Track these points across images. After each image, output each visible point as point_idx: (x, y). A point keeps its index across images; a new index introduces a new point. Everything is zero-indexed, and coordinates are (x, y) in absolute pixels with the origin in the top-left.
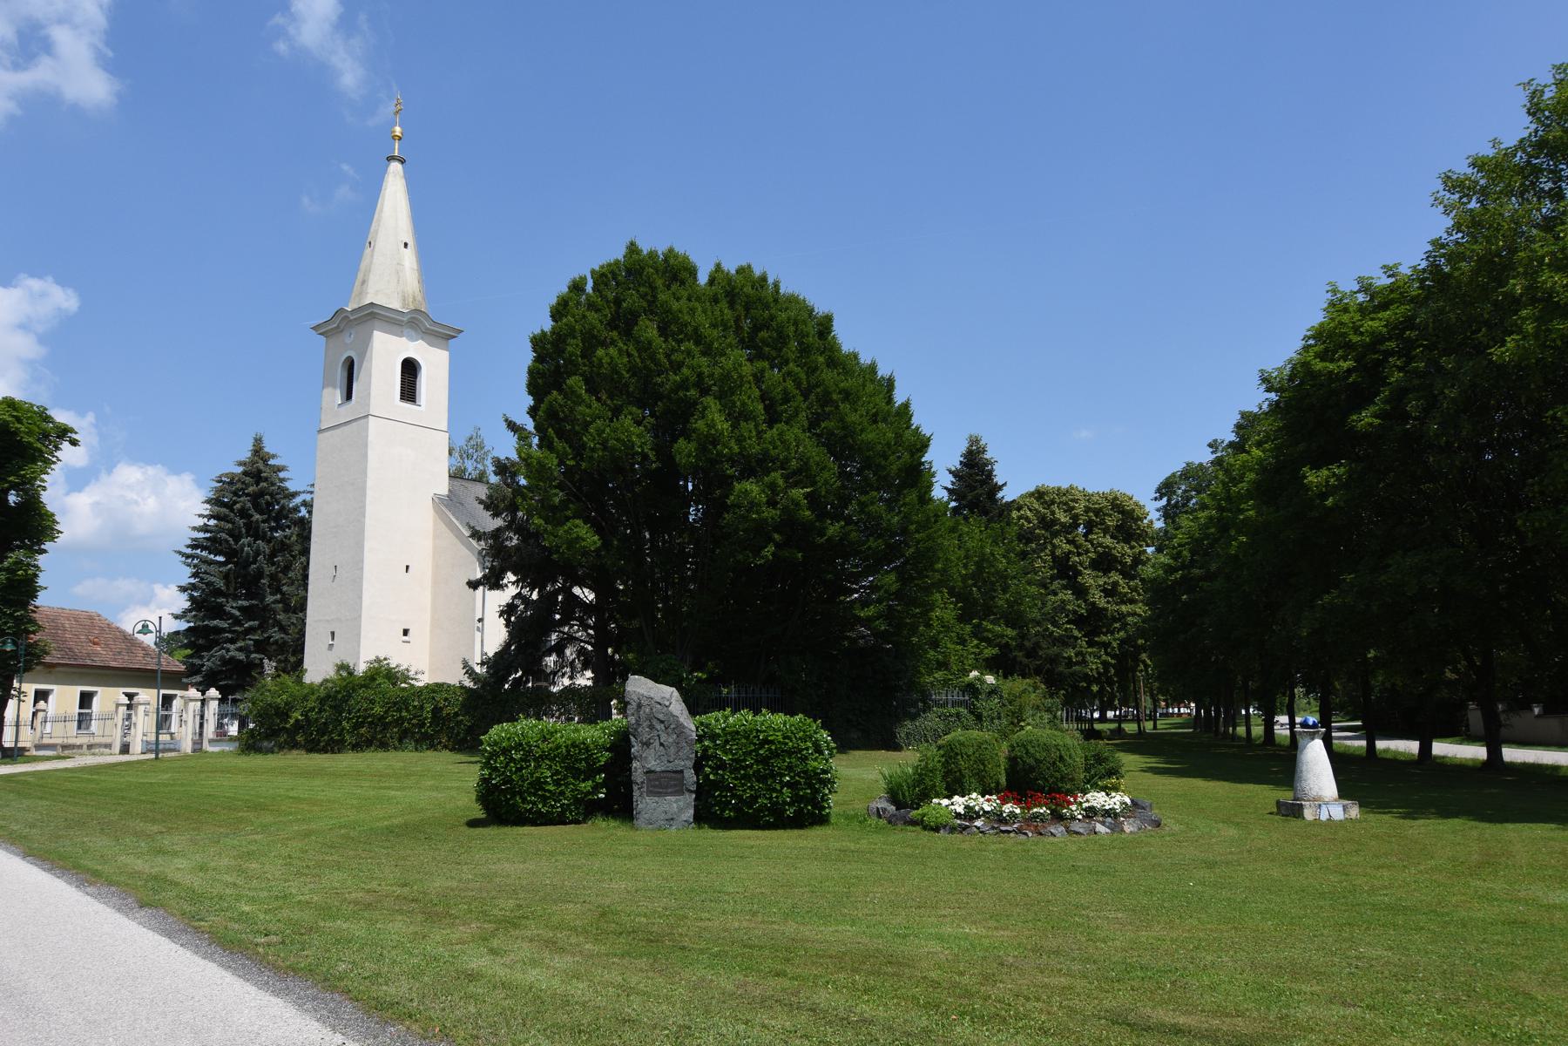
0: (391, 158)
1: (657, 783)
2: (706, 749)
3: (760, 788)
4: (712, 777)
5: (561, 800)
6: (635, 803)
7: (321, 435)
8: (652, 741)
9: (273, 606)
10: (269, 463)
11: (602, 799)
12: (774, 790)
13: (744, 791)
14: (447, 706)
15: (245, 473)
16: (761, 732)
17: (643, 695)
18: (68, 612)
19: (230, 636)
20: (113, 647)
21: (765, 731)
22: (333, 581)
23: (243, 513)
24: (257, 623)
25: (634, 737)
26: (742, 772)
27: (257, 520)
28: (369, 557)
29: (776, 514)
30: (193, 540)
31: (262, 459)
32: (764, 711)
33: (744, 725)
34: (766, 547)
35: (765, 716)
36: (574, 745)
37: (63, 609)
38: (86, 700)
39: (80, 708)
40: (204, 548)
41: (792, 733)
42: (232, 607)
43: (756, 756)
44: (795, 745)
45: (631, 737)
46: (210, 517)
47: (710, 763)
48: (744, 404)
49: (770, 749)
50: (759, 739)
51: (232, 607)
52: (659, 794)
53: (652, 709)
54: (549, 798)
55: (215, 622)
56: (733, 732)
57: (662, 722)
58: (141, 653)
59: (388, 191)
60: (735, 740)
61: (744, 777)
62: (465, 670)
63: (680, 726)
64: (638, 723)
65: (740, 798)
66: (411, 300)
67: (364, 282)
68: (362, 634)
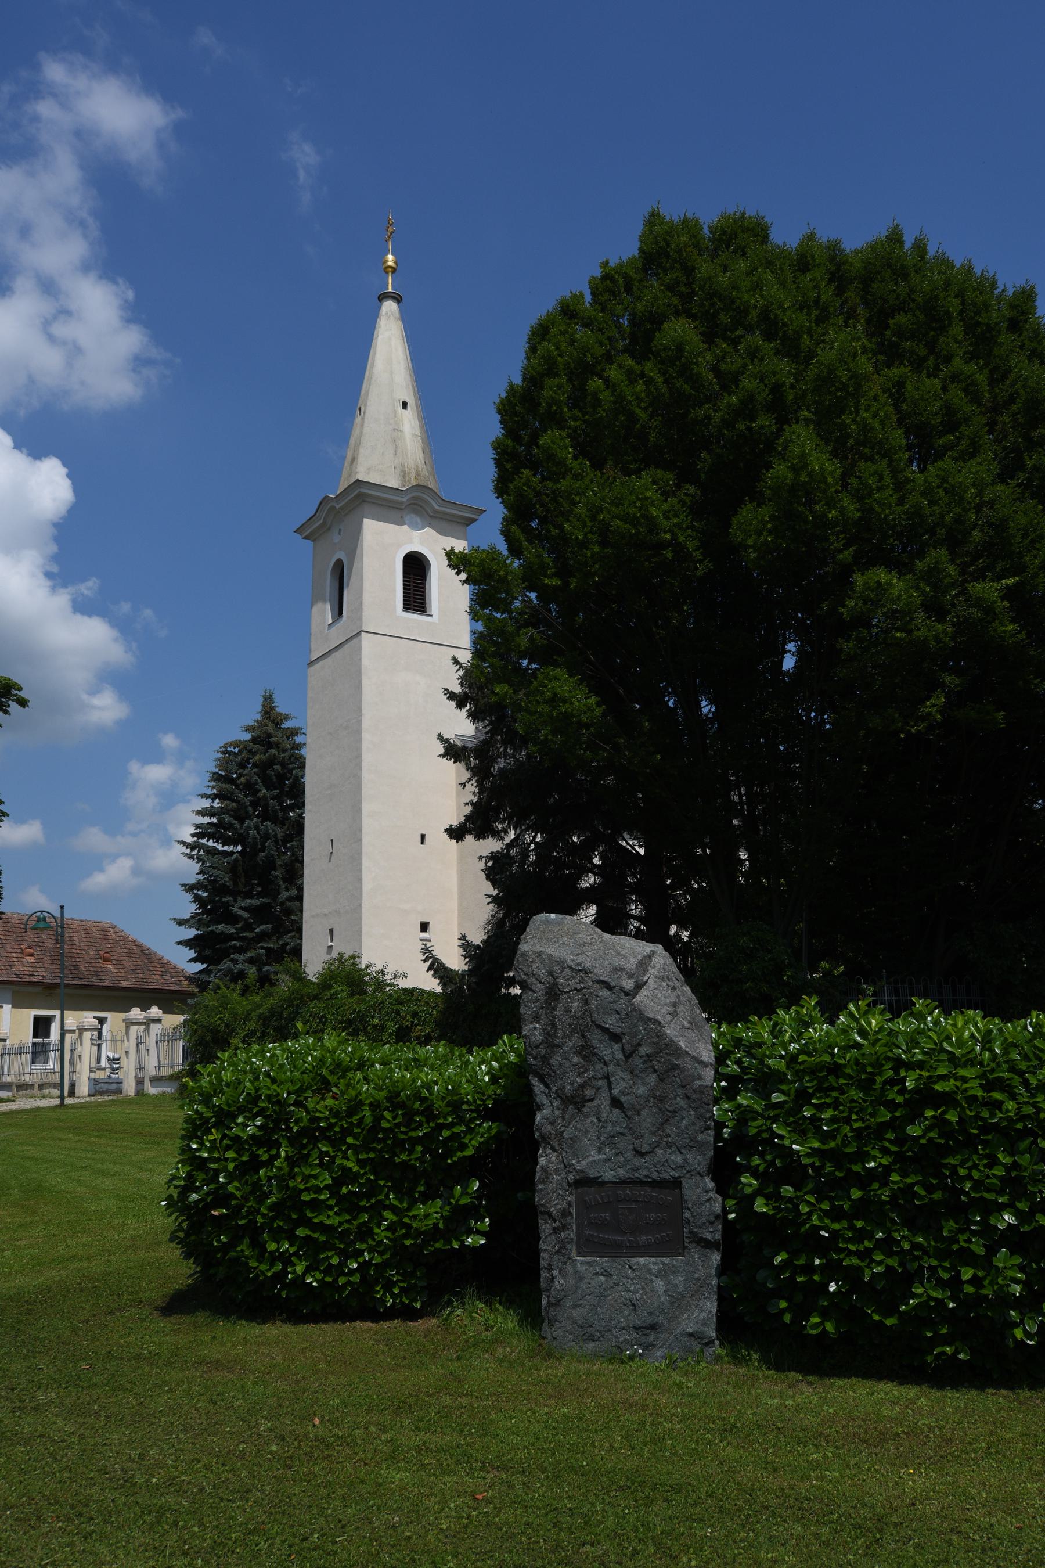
0: (383, 297)
1: (606, 1215)
2: (744, 1116)
3: (916, 1246)
4: (760, 1206)
5: (360, 1253)
6: (544, 1274)
7: (312, 668)
8: (589, 1093)
9: (289, 904)
10: (283, 726)
11: (474, 1250)
12: (967, 1257)
13: (865, 1255)
14: (416, 1025)
15: (254, 740)
16: (910, 1066)
17: (562, 963)
18: (79, 922)
19: (238, 944)
20: (126, 963)
21: (920, 1065)
22: (330, 861)
23: (250, 787)
24: (270, 926)
25: (542, 1079)
26: (856, 1194)
27: (264, 797)
28: (368, 824)
29: (945, 631)
30: (198, 826)
31: (273, 721)
32: (919, 1004)
33: (857, 1046)
34: (928, 698)
35: (921, 1017)
36: (394, 1100)
37: (73, 920)
38: (41, 1026)
39: (35, 1036)
40: (210, 836)
41: (1013, 1069)
42: (239, 907)
43: (898, 1142)
44: (1029, 1110)
45: (534, 1081)
46: (214, 797)
47: (756, 1161)
48: (865, 428)
49: (940, 1122)
50: (903, 1091)
51: (239, 907)
52: (612, 1249)
53: (586, 1002)
54: (326, 1246)
55: (220, 927)
56: (821, 1067)
57: (616, 1038)
58: (159, 970)
59: (379, 338)
60: (827, 1091)
61: (861, 1209)
62: (427, 964)
63: (667, 1048)
64: (550, 1042)
65: (851, 1277)
66: (413, 475)
67: (353, 460)
68: (364, 931)
